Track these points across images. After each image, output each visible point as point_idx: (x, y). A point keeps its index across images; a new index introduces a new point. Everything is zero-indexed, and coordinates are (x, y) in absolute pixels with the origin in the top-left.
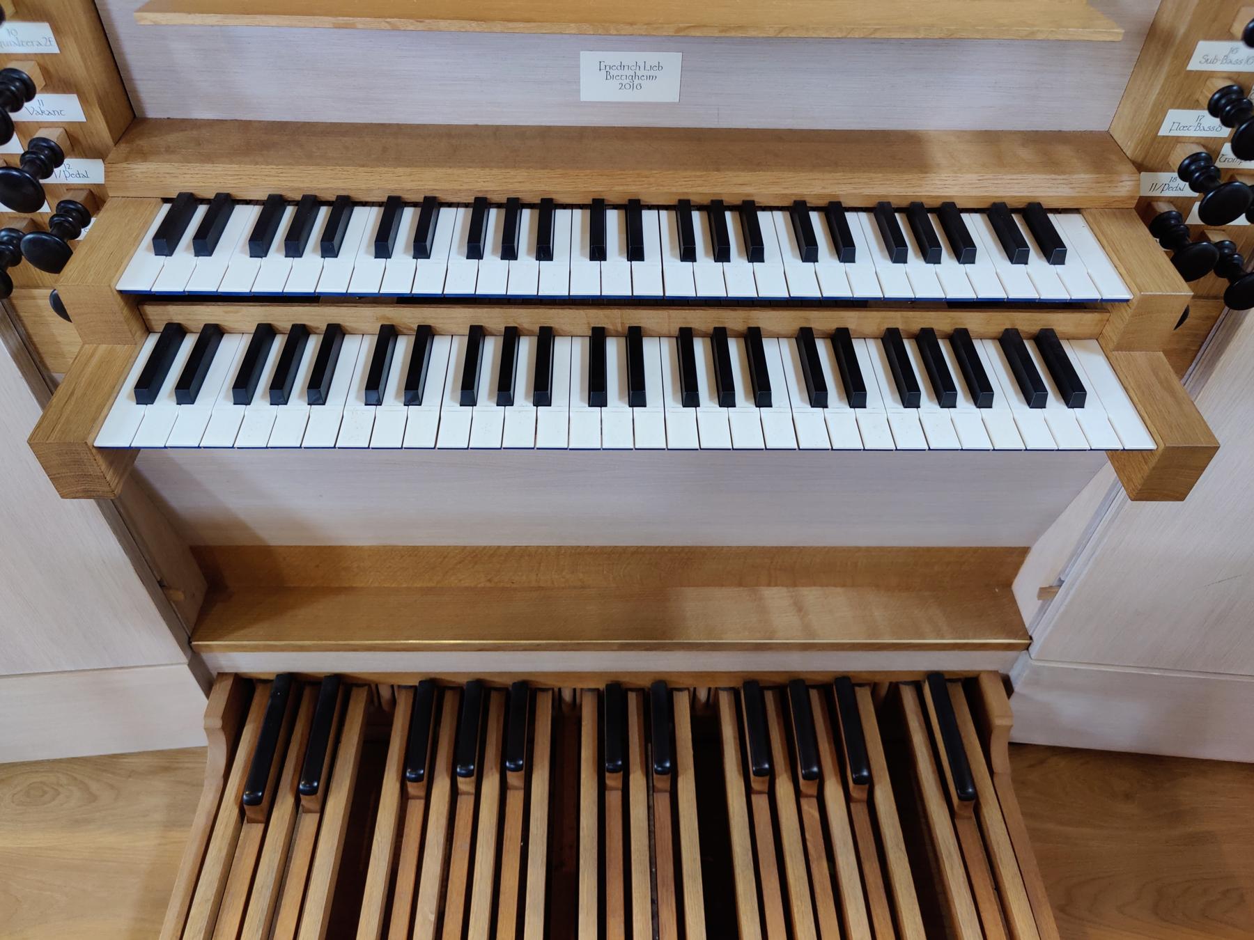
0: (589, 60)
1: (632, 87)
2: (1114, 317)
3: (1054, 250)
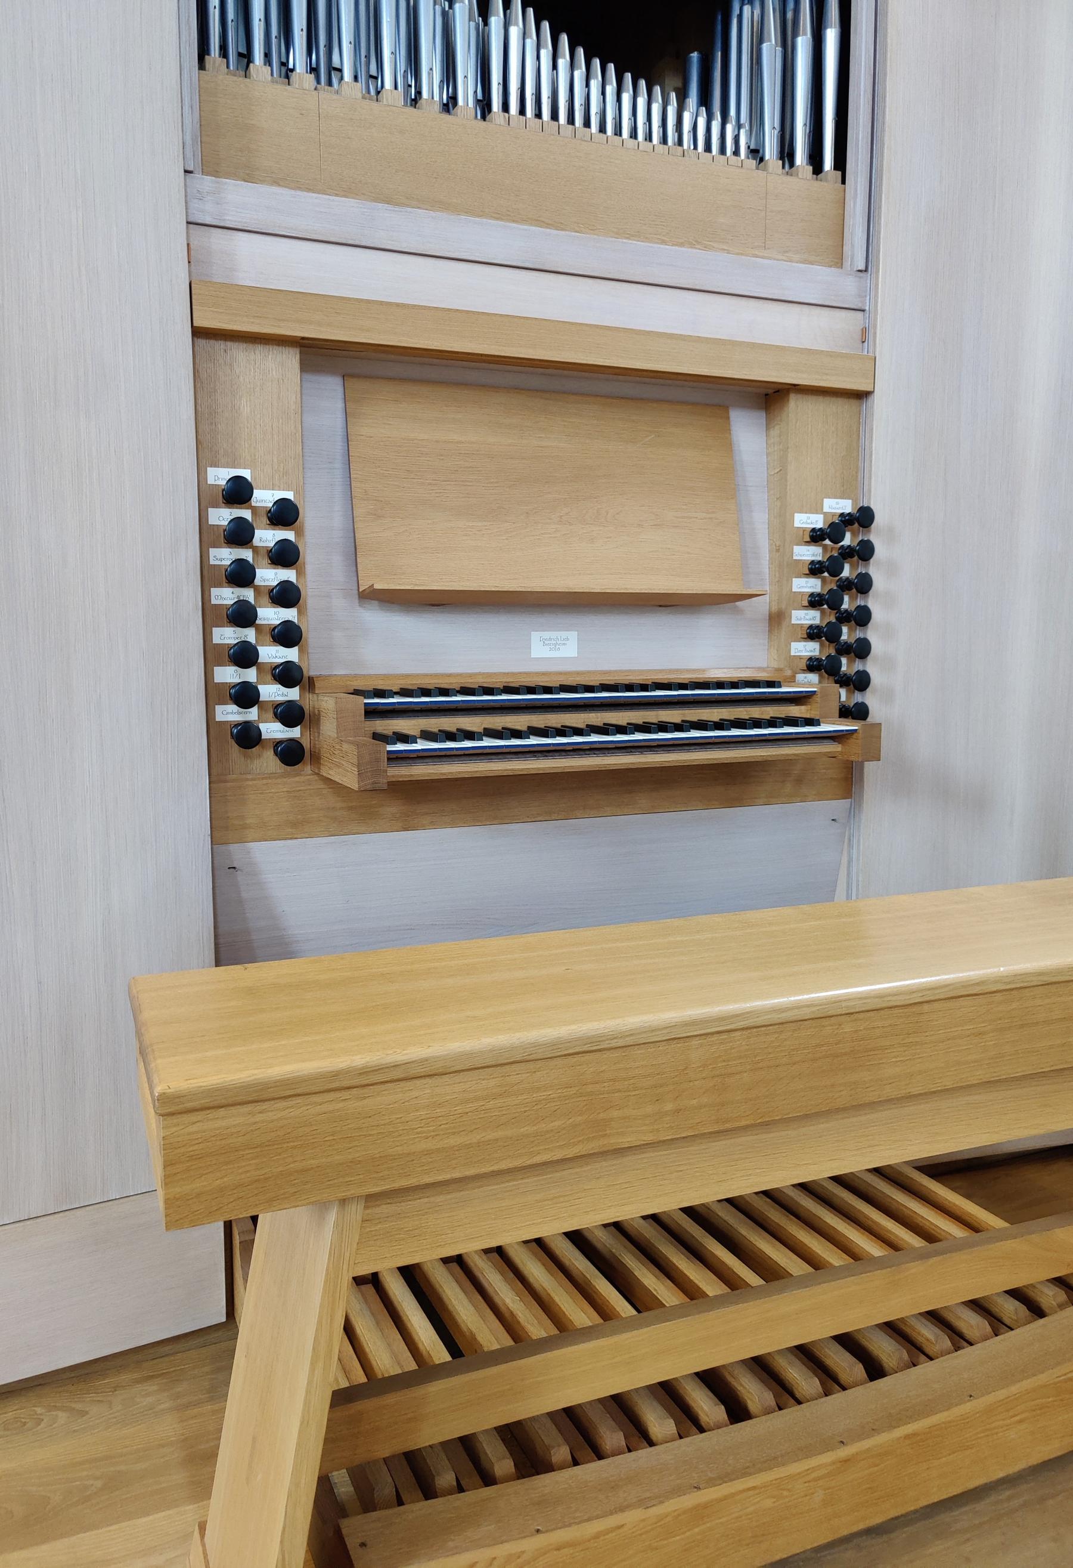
0: (535, 636)
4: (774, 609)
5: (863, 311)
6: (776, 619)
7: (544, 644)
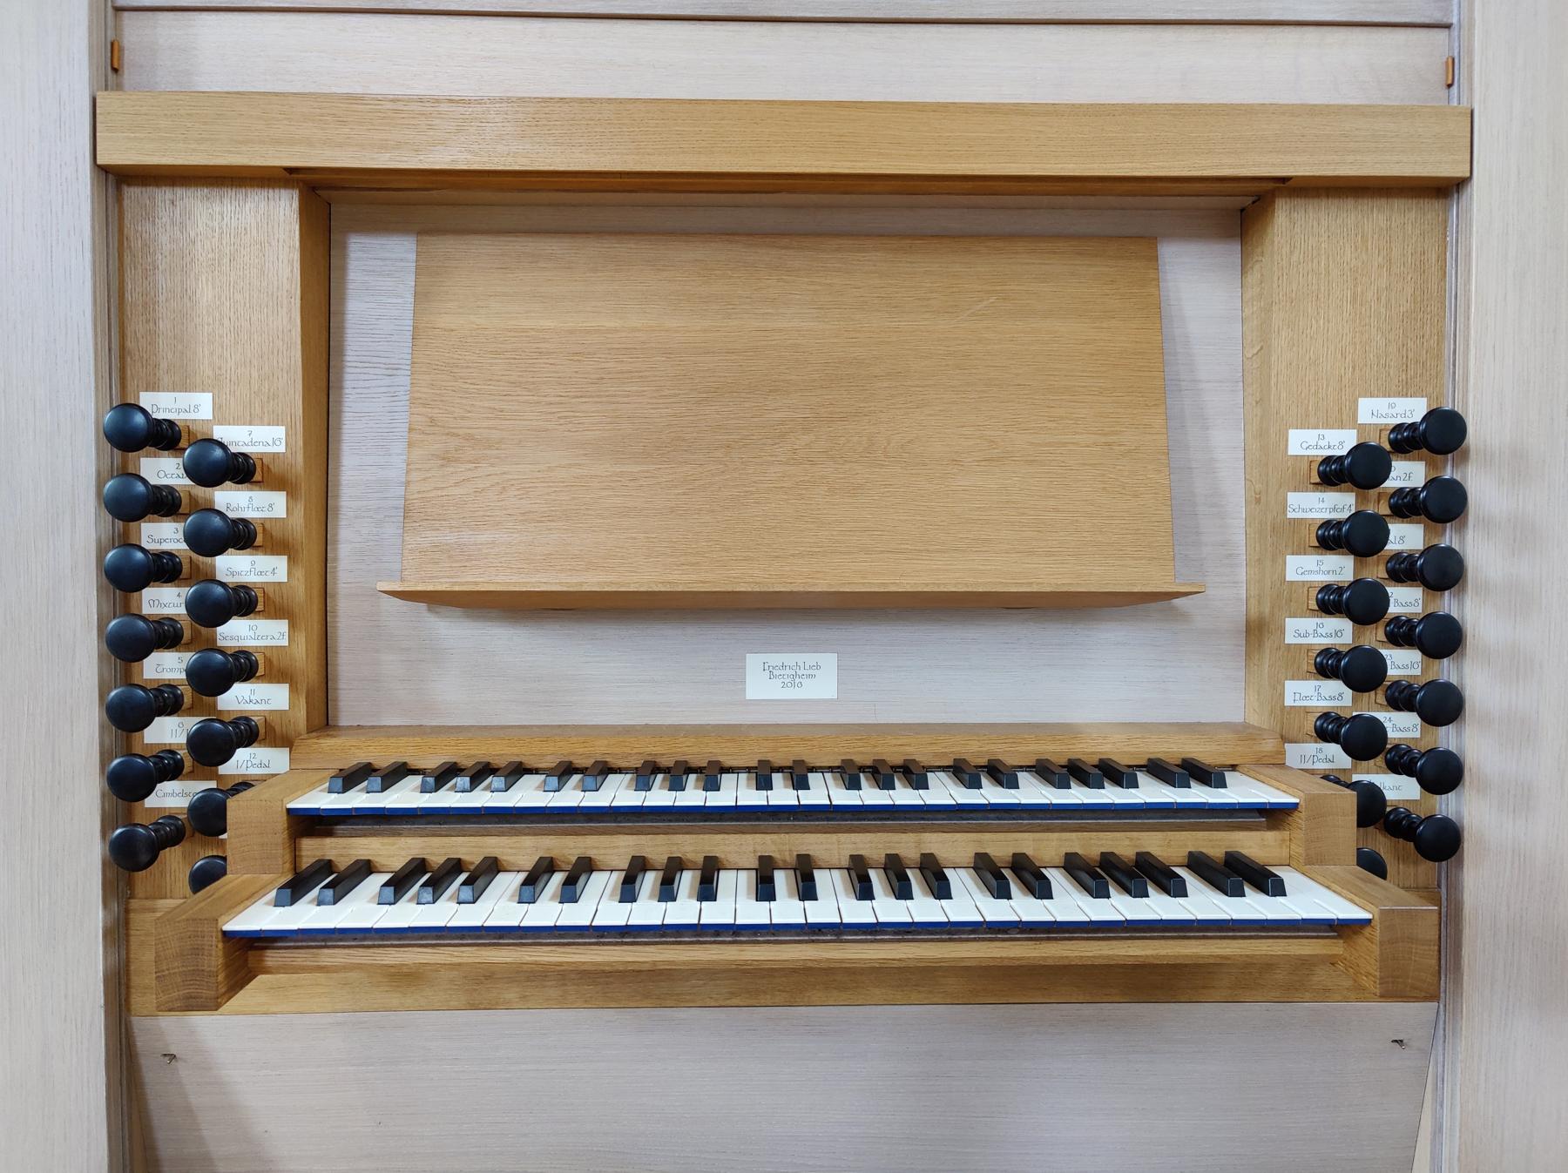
0: (754, 661)
1: (793, 685)
2: (1361, 941)
3: (1278, 889)
4: (1254, 613)
5: (1448, 26)
6: (1258, 631)
7: (772, 676)
